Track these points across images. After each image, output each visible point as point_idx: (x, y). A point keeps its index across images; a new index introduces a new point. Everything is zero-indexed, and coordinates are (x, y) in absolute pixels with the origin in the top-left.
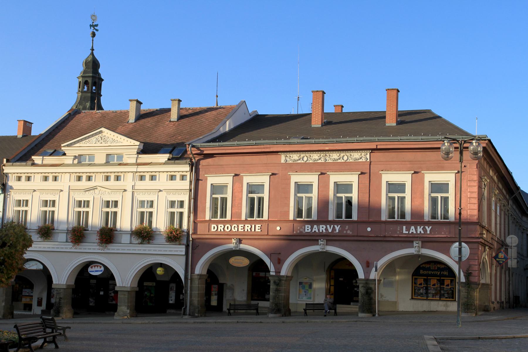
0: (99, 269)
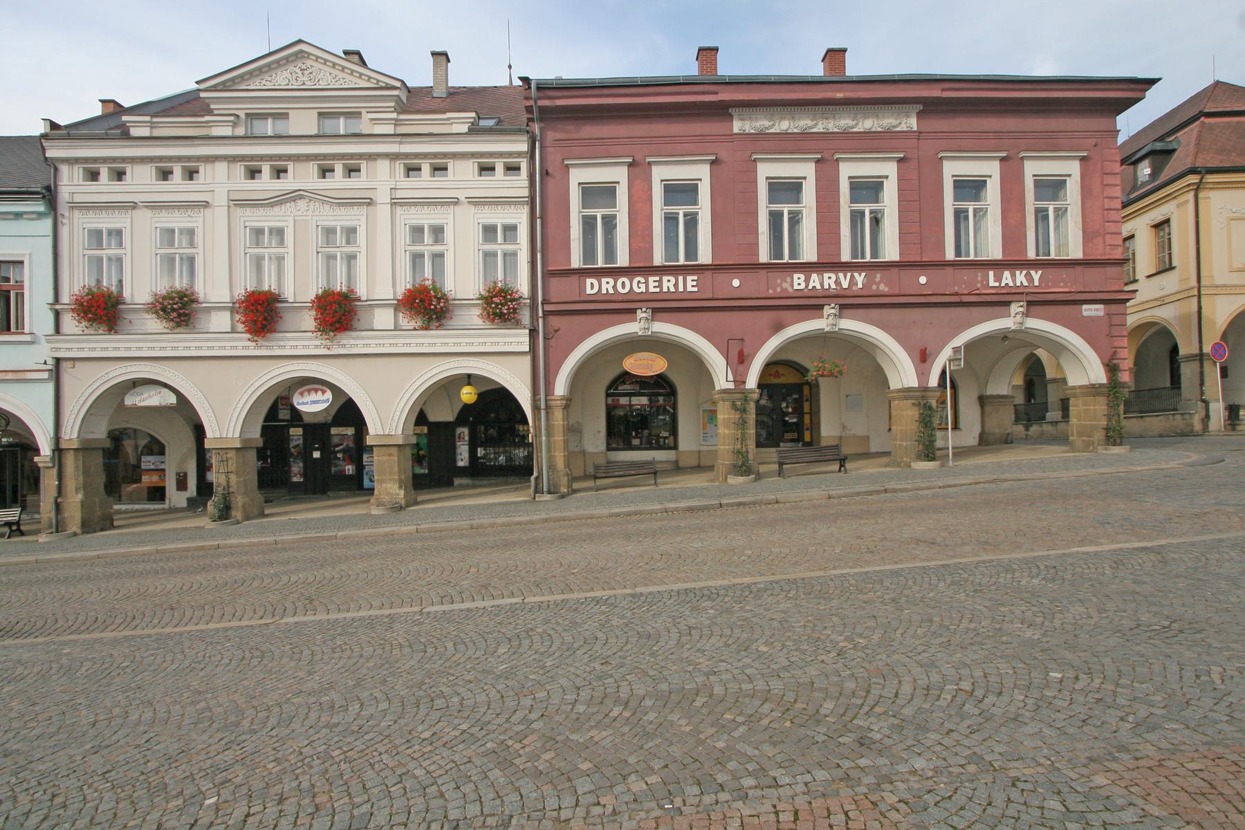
0: (319, 396)
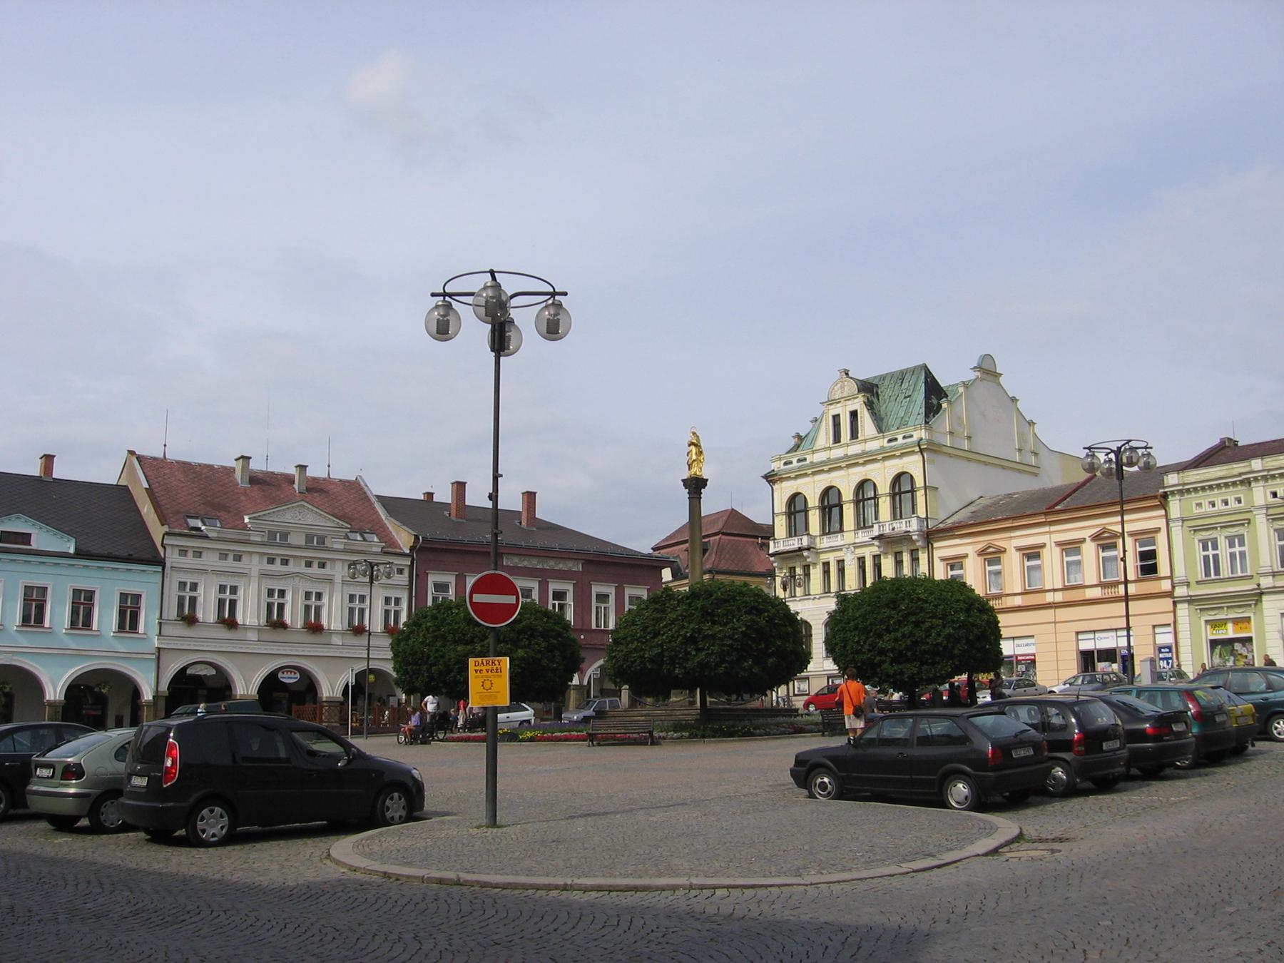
0: (293, 675)
